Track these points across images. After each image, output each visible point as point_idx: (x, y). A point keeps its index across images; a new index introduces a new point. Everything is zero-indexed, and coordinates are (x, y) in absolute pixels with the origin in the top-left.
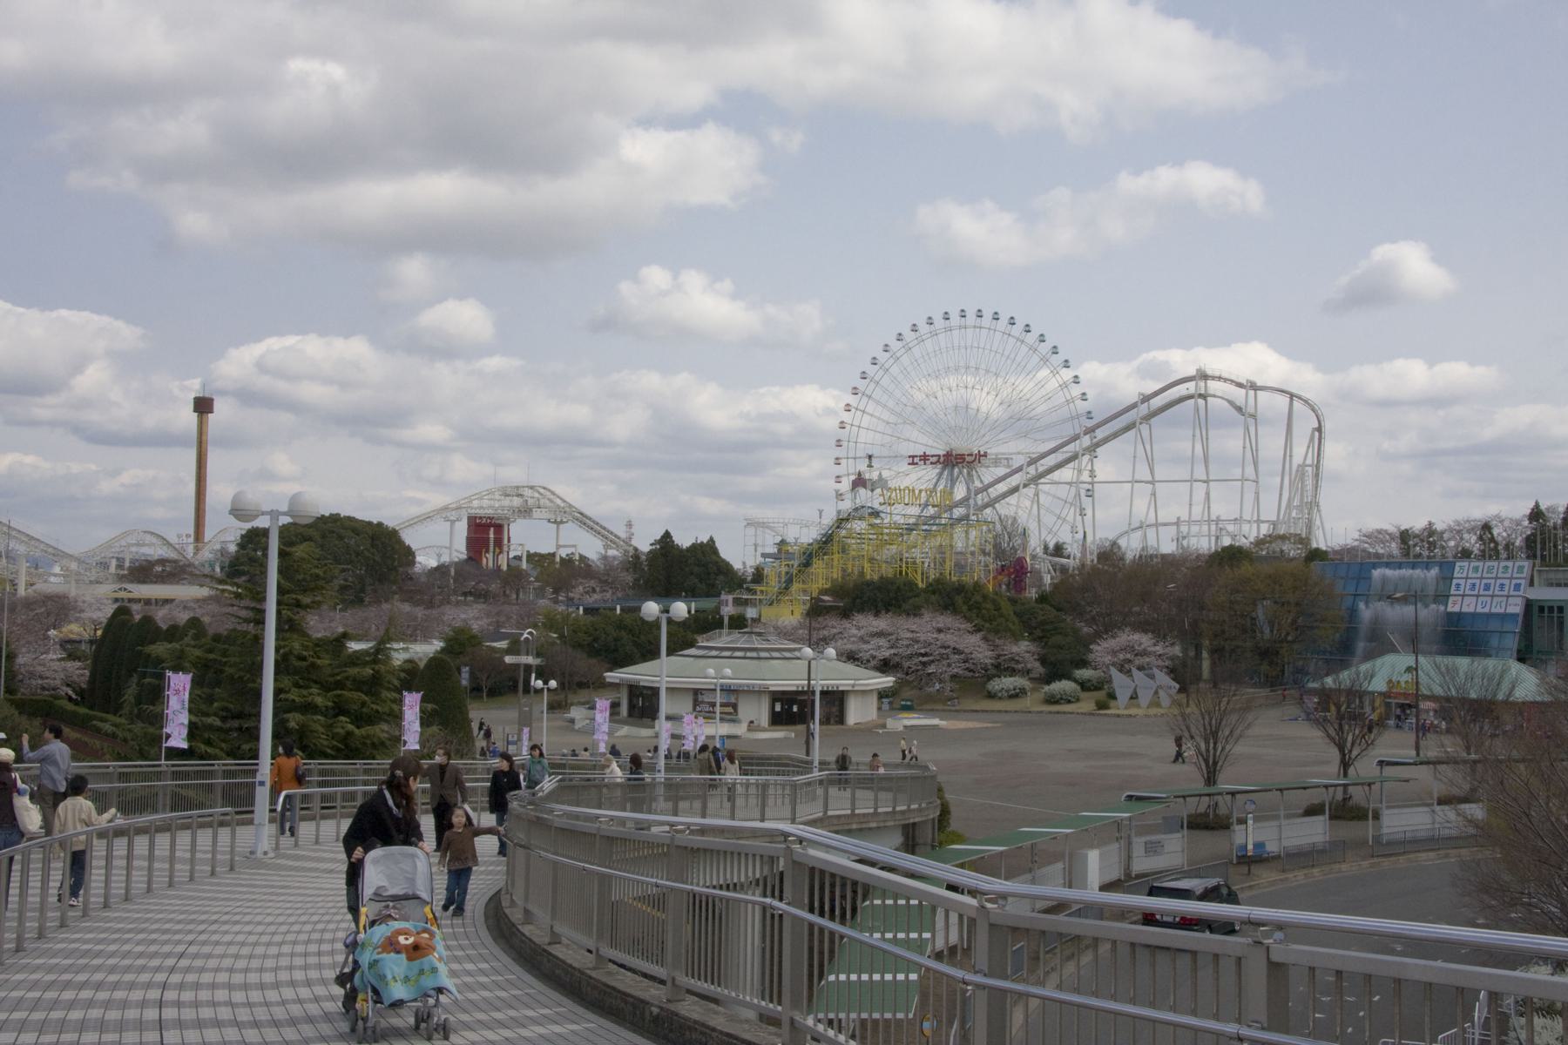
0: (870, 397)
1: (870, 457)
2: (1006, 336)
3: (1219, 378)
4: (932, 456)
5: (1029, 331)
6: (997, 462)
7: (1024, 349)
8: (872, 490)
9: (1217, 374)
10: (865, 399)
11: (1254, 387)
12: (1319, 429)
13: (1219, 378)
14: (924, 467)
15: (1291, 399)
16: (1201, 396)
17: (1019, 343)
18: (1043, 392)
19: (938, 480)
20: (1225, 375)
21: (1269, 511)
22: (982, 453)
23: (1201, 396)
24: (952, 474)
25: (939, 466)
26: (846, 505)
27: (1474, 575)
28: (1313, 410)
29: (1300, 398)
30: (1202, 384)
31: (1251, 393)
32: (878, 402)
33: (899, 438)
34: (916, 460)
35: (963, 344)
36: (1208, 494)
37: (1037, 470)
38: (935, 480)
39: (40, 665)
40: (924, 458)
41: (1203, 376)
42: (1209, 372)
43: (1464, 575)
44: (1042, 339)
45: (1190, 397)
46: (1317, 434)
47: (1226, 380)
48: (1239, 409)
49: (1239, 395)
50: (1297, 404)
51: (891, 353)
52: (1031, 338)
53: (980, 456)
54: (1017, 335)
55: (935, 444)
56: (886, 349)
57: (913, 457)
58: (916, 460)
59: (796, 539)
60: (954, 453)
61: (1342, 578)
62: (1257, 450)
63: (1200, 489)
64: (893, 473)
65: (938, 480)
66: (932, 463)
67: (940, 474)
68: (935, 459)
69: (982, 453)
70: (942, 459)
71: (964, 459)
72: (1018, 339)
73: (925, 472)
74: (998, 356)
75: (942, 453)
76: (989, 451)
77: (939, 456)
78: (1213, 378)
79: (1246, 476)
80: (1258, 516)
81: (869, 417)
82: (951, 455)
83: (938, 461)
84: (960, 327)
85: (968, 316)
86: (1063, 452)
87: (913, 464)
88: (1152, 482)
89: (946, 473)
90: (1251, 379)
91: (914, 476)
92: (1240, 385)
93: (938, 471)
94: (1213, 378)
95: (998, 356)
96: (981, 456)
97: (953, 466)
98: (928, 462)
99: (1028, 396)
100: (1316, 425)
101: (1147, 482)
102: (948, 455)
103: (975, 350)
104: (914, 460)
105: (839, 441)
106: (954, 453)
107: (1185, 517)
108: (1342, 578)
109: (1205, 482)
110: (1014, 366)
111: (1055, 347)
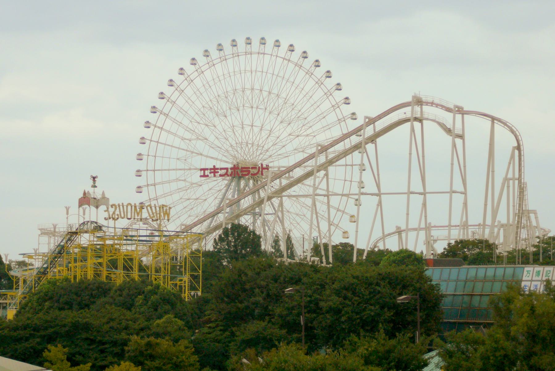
0: (167, 115)
1: (94, 178)
2: (286, 62)
3: (432, 104)
4: (221, 169)
5: (306, 57)
6: (279, 175)
7: (302, 73)
8: (97, 207)
9: (430, 100)
10: (163, 117)
11: (460, 111)
12: (519, 148)
13: (432, 104)
14: (215, 179)
15: (493, 123)
16: (416, 119)
17: (297, 68)
18: (318, 111)
19: (227, 191)
20: (436, 101)
21: (475, 218)
22: (264, 166)
23: (416, 119)
24: (238, 184)
25: (228, 178)
26: (75, 221)
27: (537, 278)
28: (512, 132)
29: (500, 120)
30: (417, 109)
31: (459, 117)
32: (174, 120)
33: (192, 152)
34: (207, 173)
35: (248, 68)
36: (424, 204)
37: (281, 183)
38: (223, 191)
39: (80, 354)
40: (214, 170)
41: (419, 102)
42: (424, 99)
43: (530, 278)
44: (317, 64)
45: (407, 120)
46: (517, 152)
47: (437, 105)
48: (449, 131)
49: (447, 118)
50: (498, 127)
51: (186, 76)
52: (308, 63)
53: (263, 169)
54: (296, 60)
55: (224, 159)
56: (182, 71)
57: (204, 170)
58: (207, 173)
59: (36, 250)
60: (240, 166)
61: (445, 281)
62: (465, 167)
63: (417, 200)
64: (187, 184)
65: (227, 191)
66: (221, 175)
67: (228, 186)
68: (224, 172)
69: (264, 166)
70: (230, 171)
71: (249, 171)
72: (296, 65)
73: (216, 182)
74: (279, 79)
75: (230, 166)
76: (270, 165)
77: (227, 169)
78: (427, 103)
79: (454, 189)
80: (447, 226)
81: (166, 134)
82: (238, 168)
83: (226, 174)
84: (246, 53)
85: (238, 45)
86: (305, 167)
87: (204, 176)
88: (379, 195)
89: (233, 184)
90: (459, 104)
91: (205, 187)
92: (448, 110)
93: (226, 182)
94: (427, 103)
95: (279, 79)
96: (263, 169)
97: (240, 178)
98: (217, 174)
99: (306, 115)
100: (516, 144)
101: (420, 194)
102: (235, 168)
103: (259, 74)
104: (205, 173)
105: (140, 155)
106: (240, 166)
107: (403, 227)
108: (445, 281)
109: (455, 192)
110: (293, 88)
111: (328, 72)
